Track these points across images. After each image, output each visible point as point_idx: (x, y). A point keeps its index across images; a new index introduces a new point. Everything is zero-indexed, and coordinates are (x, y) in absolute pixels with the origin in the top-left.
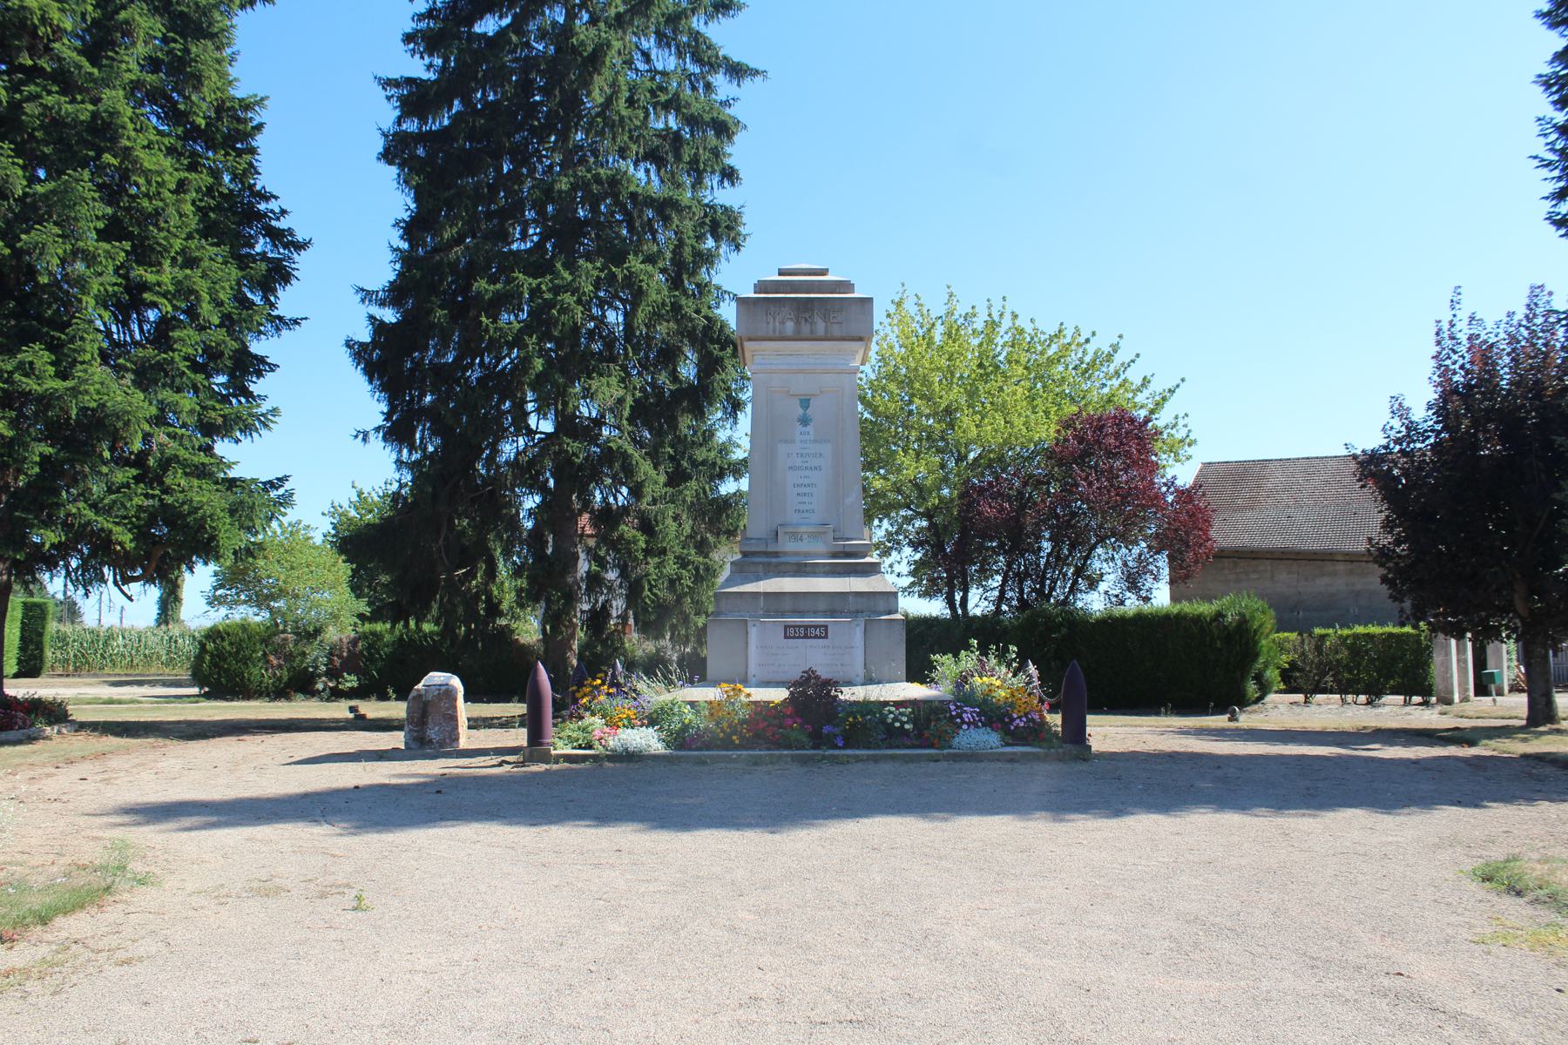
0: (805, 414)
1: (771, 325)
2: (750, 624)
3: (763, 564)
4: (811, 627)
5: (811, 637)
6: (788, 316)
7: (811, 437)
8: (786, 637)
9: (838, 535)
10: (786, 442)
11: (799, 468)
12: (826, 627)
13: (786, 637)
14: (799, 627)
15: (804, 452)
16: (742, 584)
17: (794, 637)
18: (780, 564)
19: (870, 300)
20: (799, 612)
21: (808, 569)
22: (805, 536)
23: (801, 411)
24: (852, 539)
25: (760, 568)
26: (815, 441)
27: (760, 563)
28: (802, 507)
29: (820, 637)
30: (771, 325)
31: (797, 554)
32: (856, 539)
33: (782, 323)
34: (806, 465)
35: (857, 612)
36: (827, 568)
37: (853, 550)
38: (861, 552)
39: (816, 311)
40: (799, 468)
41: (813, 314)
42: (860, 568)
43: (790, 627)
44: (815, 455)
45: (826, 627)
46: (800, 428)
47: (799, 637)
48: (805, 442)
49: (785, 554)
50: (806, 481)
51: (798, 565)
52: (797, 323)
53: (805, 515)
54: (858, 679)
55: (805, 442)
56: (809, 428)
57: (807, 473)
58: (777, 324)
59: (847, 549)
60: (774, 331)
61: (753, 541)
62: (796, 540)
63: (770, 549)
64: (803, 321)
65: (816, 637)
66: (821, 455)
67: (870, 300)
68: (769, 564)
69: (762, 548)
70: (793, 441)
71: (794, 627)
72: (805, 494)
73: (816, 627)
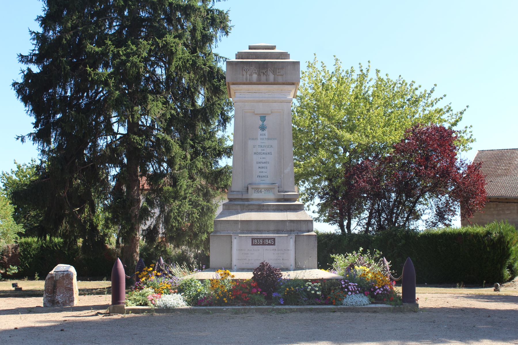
0: (263, 124)
1: (245, 77)
2: (233, 238)
3: (240, 205)
4: (266, 239)
5: (266, 245)
6: (254, 72)
7: (266, 137)
8: (252, 245)
9: (281, 189)
10: (253, 139)
11: (260, 153)
12: (274, 239)
13: (252, 245)
14: (260, 239)
15: (263, 144)
16: (229, 216)
17: (257, 245)
18: (249, 205)
19: (298, 63)
20: (259, 231)
21: (265, 208)
22: (263, 190)
23: (261, 123)
24: (288, 192)
25: (239, 207)
26: (268, 139)
27: (239, 204)
28: (261, 174)
29: (271, 245)
30: (245, 77)
31: (258, 200)
32: (290, 192)
33: (251, 75)
34: (263, 152)
35: (291, 231)
36: (275, 208)
37: (289, 197)
38: (293, 199)
39: (269, 69)
40: (260, 153)
41: (267, 70)
42: (293, 207)
43: (255, 239)
44: (268, 147)
45: (274, 239)
46: (260, 132)
47: (260, 245)
48: (263, 139)
49: (252, 199)
50: (264, 160)
51: (260, 205)
52: (259, 75)
53: (263, 179)
54: (292, 267)
55: (263, 139)
56: (265, 132)
57: (264, 156)
58: (248, 76)
59: (285, 197)
60: (246, 79)
61: (235, 193)
62: (258, 192)
63: (244, 197)
64: (262, 74)
65: (269, 244)
66: (271, 146)
67: (298, 63)
68: (244, 205)
69: (240, 197)
70: (256, 139)
71: (257, 239)
72: (263, 167)
73: (269, 239)
